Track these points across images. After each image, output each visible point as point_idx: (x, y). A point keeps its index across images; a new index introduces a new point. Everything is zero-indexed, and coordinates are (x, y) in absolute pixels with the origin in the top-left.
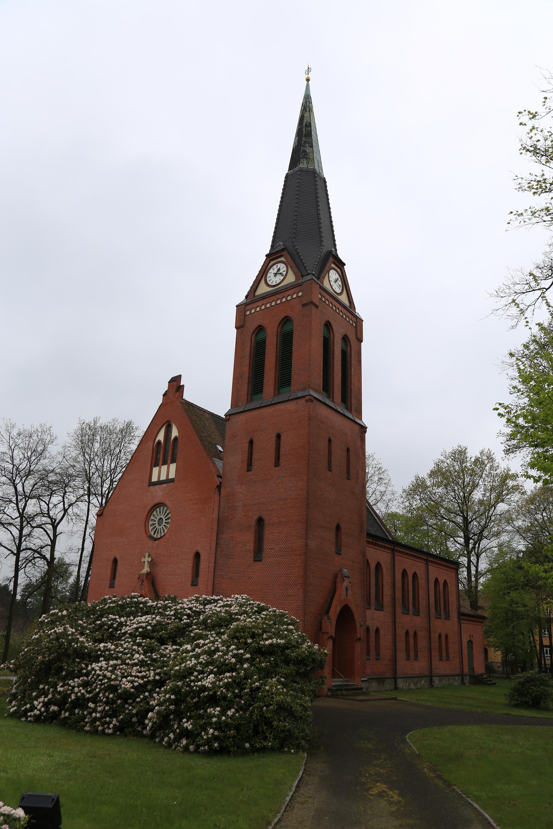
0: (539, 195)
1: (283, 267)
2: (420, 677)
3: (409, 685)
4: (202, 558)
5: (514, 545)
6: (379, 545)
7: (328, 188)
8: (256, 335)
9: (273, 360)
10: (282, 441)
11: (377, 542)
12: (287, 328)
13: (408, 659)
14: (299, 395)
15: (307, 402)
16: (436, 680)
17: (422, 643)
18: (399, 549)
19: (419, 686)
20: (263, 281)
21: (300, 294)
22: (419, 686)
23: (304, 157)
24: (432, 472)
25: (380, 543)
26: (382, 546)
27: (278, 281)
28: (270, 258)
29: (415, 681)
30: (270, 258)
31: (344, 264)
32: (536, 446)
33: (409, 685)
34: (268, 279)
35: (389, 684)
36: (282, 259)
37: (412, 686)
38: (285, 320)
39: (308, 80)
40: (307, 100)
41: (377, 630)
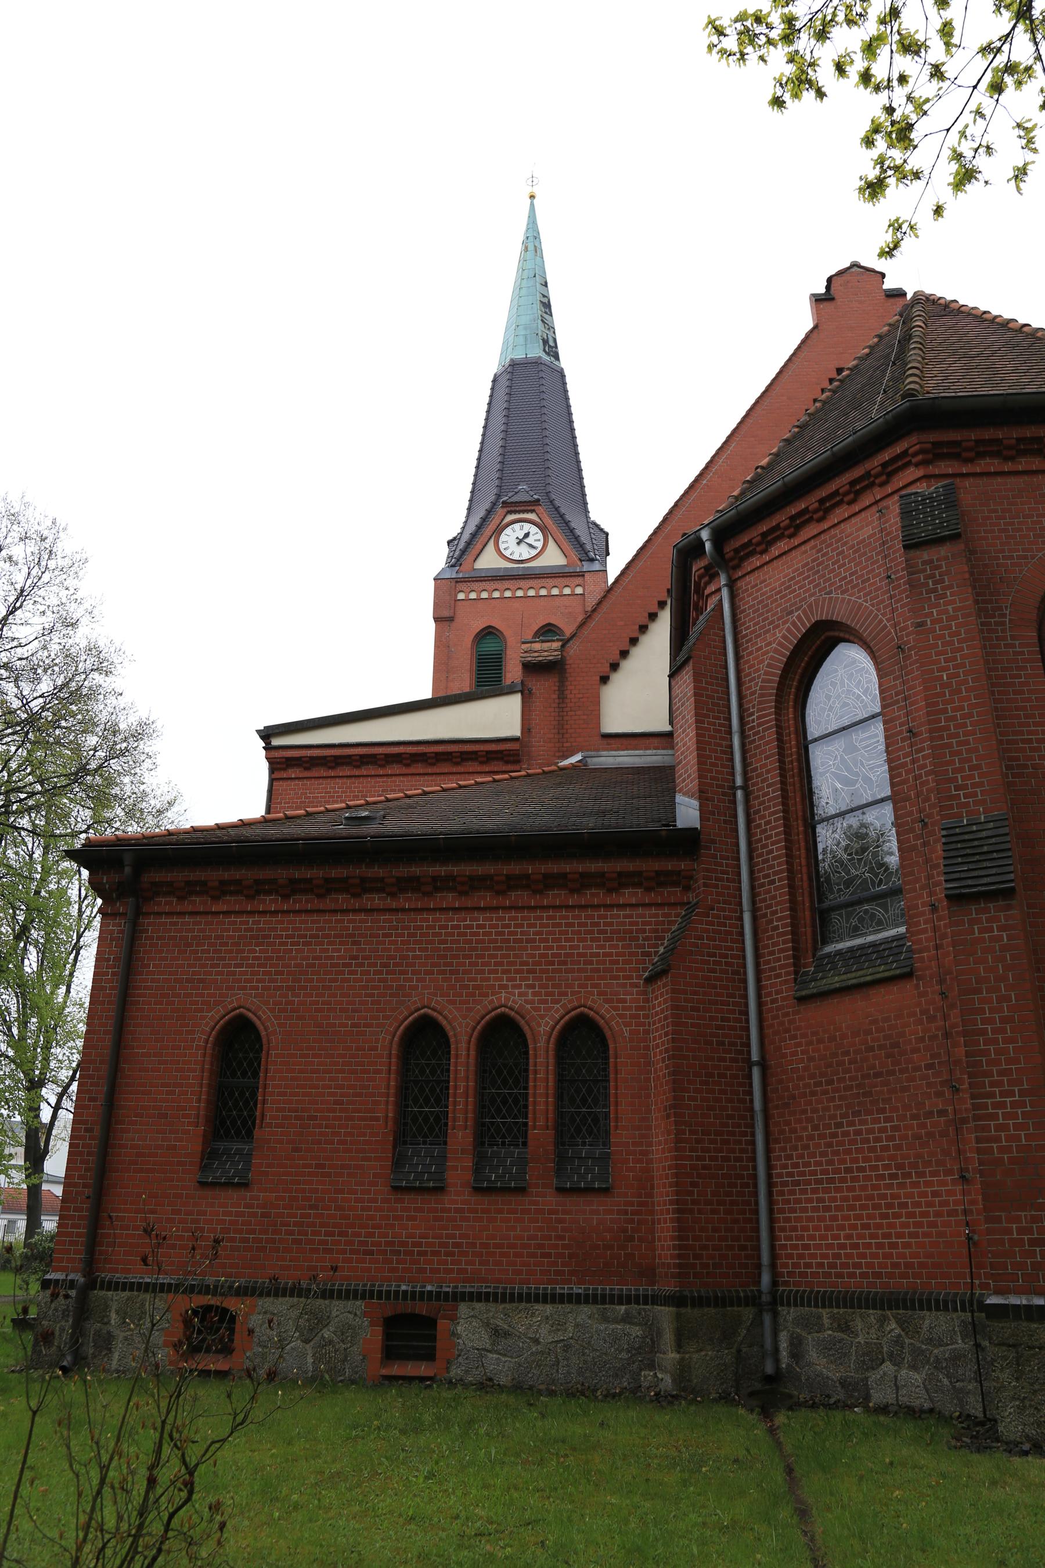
1: (536, 536)
12: (490, 646)
20: (491, 545)
21: (579, 590)
27: (525, 556)
34: (502, 546)
36: (532, 516)
39: (532, 197)
40: (532, 243)
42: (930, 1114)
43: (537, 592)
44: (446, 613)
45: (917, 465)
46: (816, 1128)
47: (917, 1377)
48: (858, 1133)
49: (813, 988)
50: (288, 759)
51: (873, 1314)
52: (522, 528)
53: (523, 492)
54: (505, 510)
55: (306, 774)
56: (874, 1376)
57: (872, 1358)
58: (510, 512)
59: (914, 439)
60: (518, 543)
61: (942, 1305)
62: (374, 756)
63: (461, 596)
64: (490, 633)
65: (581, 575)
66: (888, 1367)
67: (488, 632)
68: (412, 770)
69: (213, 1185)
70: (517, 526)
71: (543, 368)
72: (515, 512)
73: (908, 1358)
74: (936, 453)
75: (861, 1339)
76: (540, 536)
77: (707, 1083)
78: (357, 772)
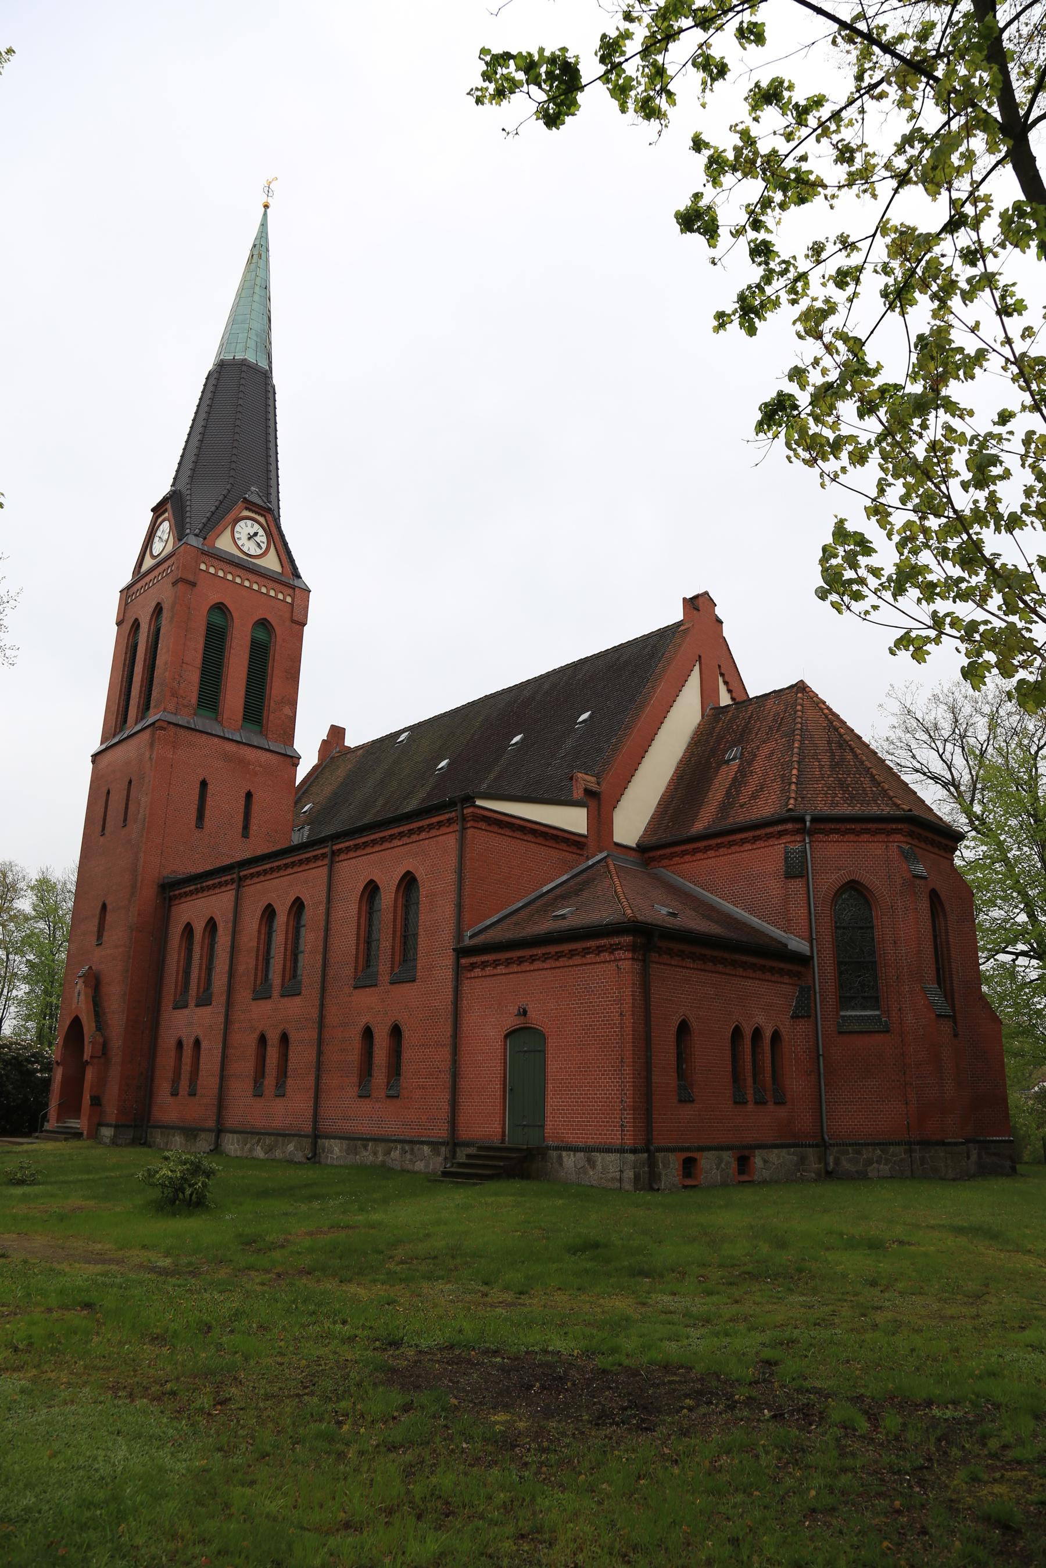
0: (711, 90)
2: (284, 1135)
3: (251, 1150)
6: (209, 888)
7: (842, 717)
11: (204, 884)
13: (258, 1094)
16: (335, 1150)
17: (301, 1056)
18: (251, 871)
19: (278, 1154)
20: (228, 531)
22: (278, 1154)
25: (210, 883)
26: (214, 886)
27: (252, 552)
29: (267, 1141)
33: (251, 1150)
34: (237, 536)
35: (204, 1143)
37: (259, 1153)
39: (266, 206)
40: (260, 252)
41: (197, 1043)
42: (894, 1081)
45: (903, 835)
46: (845, 1082)
47: (887, 1168)
48: (864, 1085)
49: (845, 1029)
50: (484, 816)
51: (870, 1148)
52: (252, 526)
54: (245, 505)
55: (488, 828)
56: (869, 1169)
57: (869, 1162)
58: (247, 509)
59: (906, 826)
60: (249, 539)
61: (898, 1144)
62: (525, 827)
63: (203, 567)
66: (875, 1165)
67: (220, 608)
68: (514, 835)
70: (249, 522)
72: (250, 510)
73: (883, 1161)
74: (911, 834)
75: (865, 1156)
76: (264, 539)
78: (500, 831)
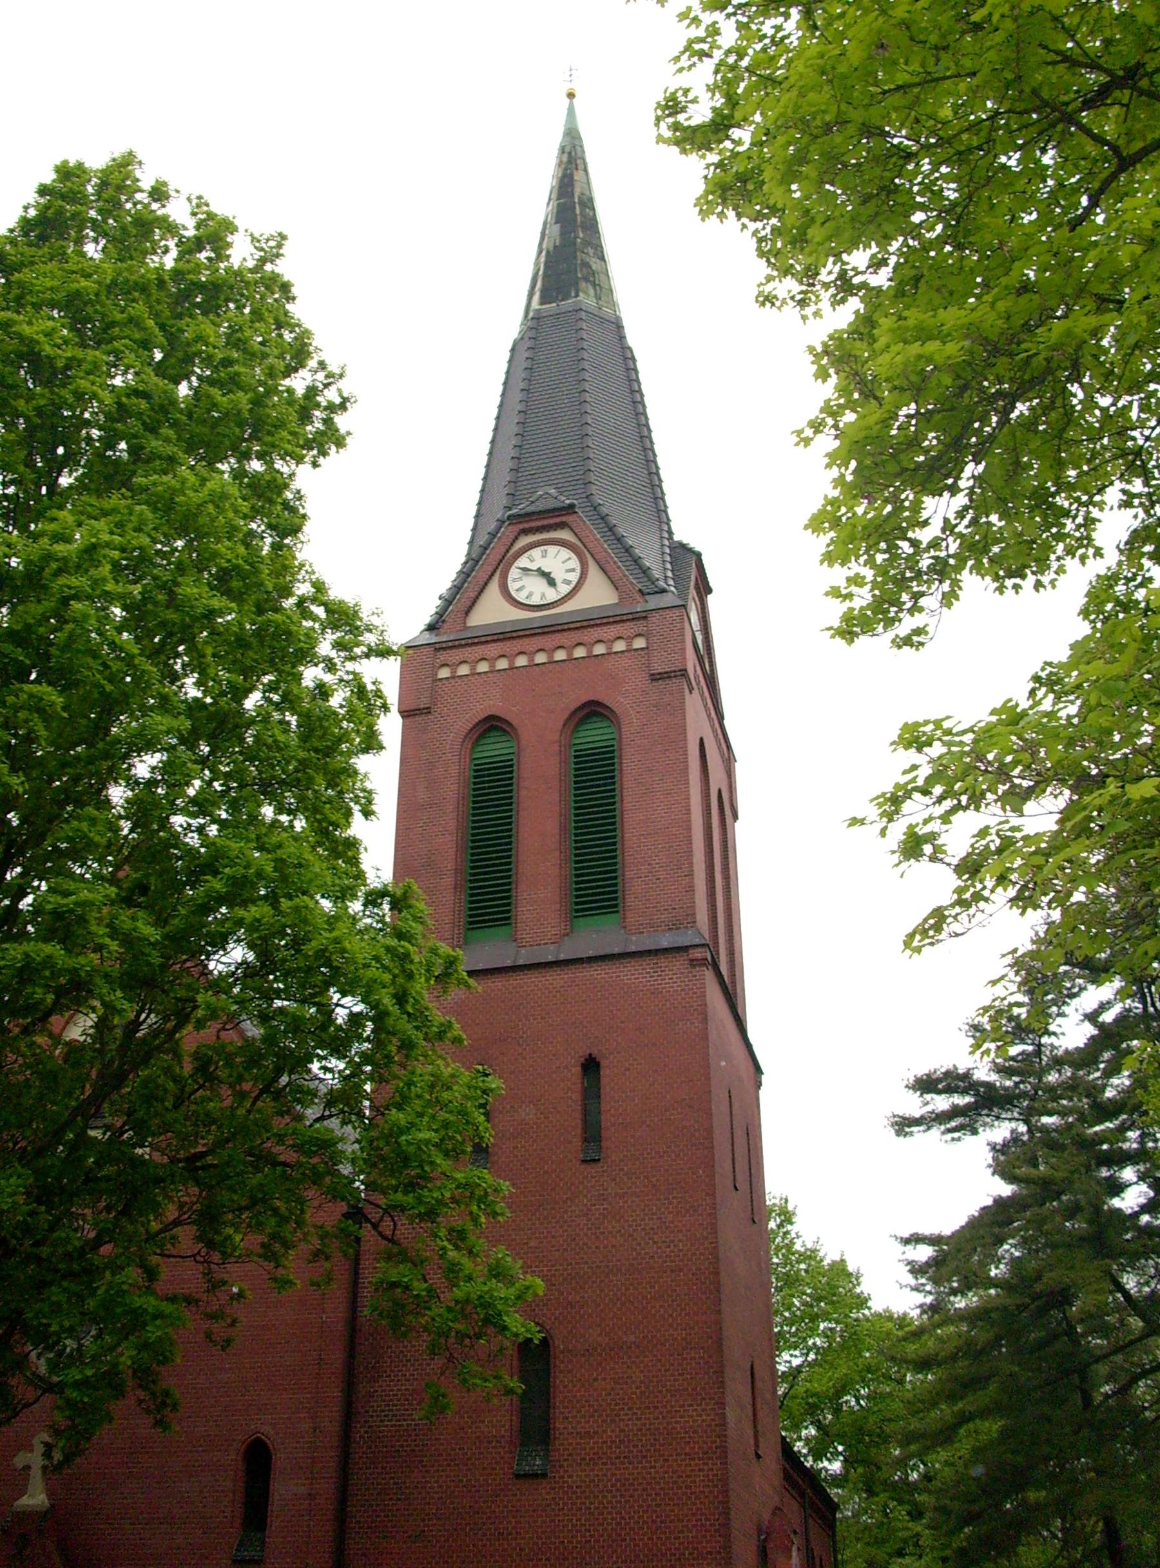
4: (280, 1459)
5: (1109, 1089)
8: (476, 743)
9: (551, 826)
10: (604, 1081)
14: (665, 943)
15: (693, 966)
20: (494, 587)
21: (639, 643)
23: (586, 280)
24: (904, 942)
28: (521, 526)
30: (521, 526)
31: (66, 172)
32: (104, 184)
34: (512, 587)
38: (587, 710)
39: (571, 95)
43: (570, 654)
44: (424, 702)
53: (548, 495)
54: (518, 528)
58: (525, 532)
64: (497, 728)
65: (643, 617)
67: (492, 725)
69: (526, 1476)
71: (583, 315)
77: (426, 1482)
